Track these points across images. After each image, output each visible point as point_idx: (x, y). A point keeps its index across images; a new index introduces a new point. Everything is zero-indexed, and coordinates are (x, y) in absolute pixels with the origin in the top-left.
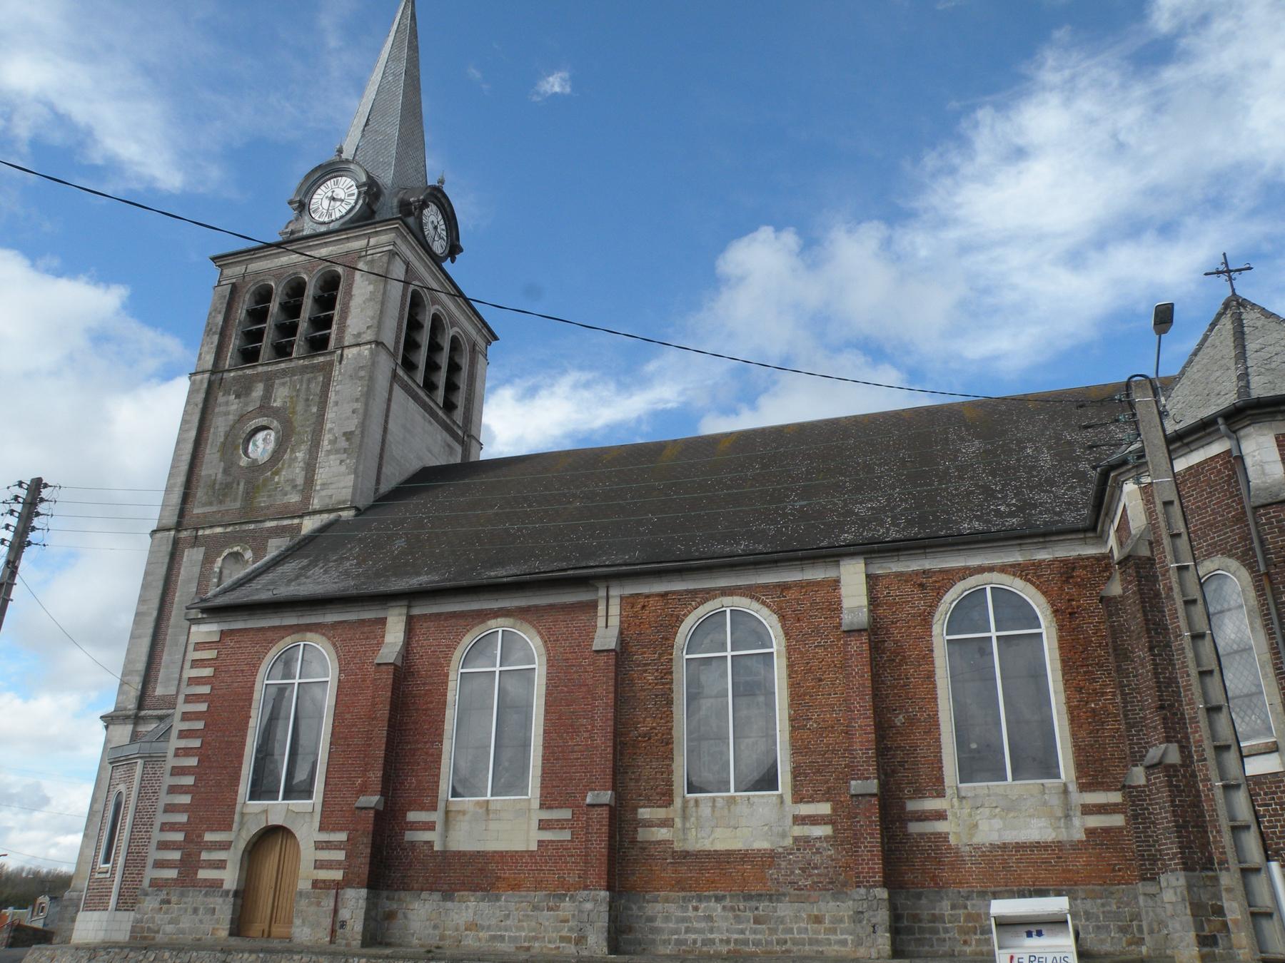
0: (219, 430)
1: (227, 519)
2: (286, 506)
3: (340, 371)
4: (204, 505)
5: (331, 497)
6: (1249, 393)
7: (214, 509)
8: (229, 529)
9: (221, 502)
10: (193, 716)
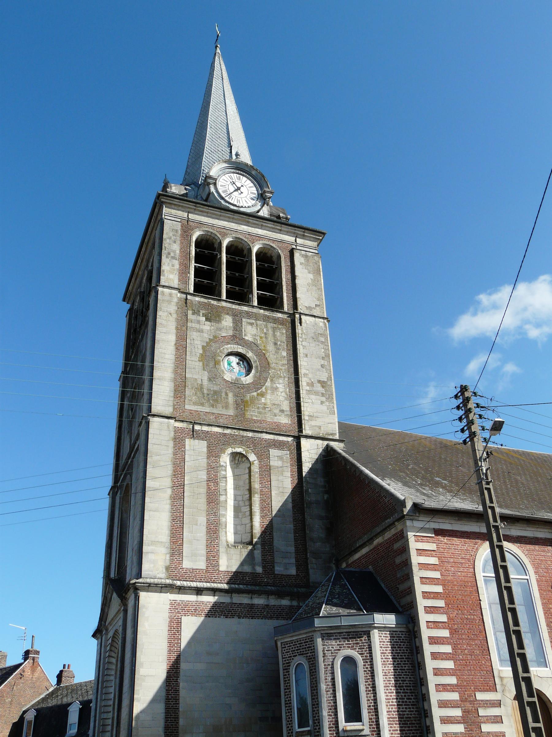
0: (196, 342)
1: (222, 421)
2: (278, 425)
3: (302, 331)
4: (195, 404)
5: (320, 427)
6: (244, 414)
7: (207, 409)
8: (228, 431)
9: (213, 406)
10: (432, 596)
